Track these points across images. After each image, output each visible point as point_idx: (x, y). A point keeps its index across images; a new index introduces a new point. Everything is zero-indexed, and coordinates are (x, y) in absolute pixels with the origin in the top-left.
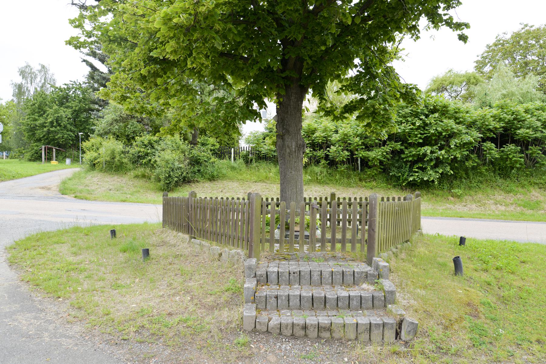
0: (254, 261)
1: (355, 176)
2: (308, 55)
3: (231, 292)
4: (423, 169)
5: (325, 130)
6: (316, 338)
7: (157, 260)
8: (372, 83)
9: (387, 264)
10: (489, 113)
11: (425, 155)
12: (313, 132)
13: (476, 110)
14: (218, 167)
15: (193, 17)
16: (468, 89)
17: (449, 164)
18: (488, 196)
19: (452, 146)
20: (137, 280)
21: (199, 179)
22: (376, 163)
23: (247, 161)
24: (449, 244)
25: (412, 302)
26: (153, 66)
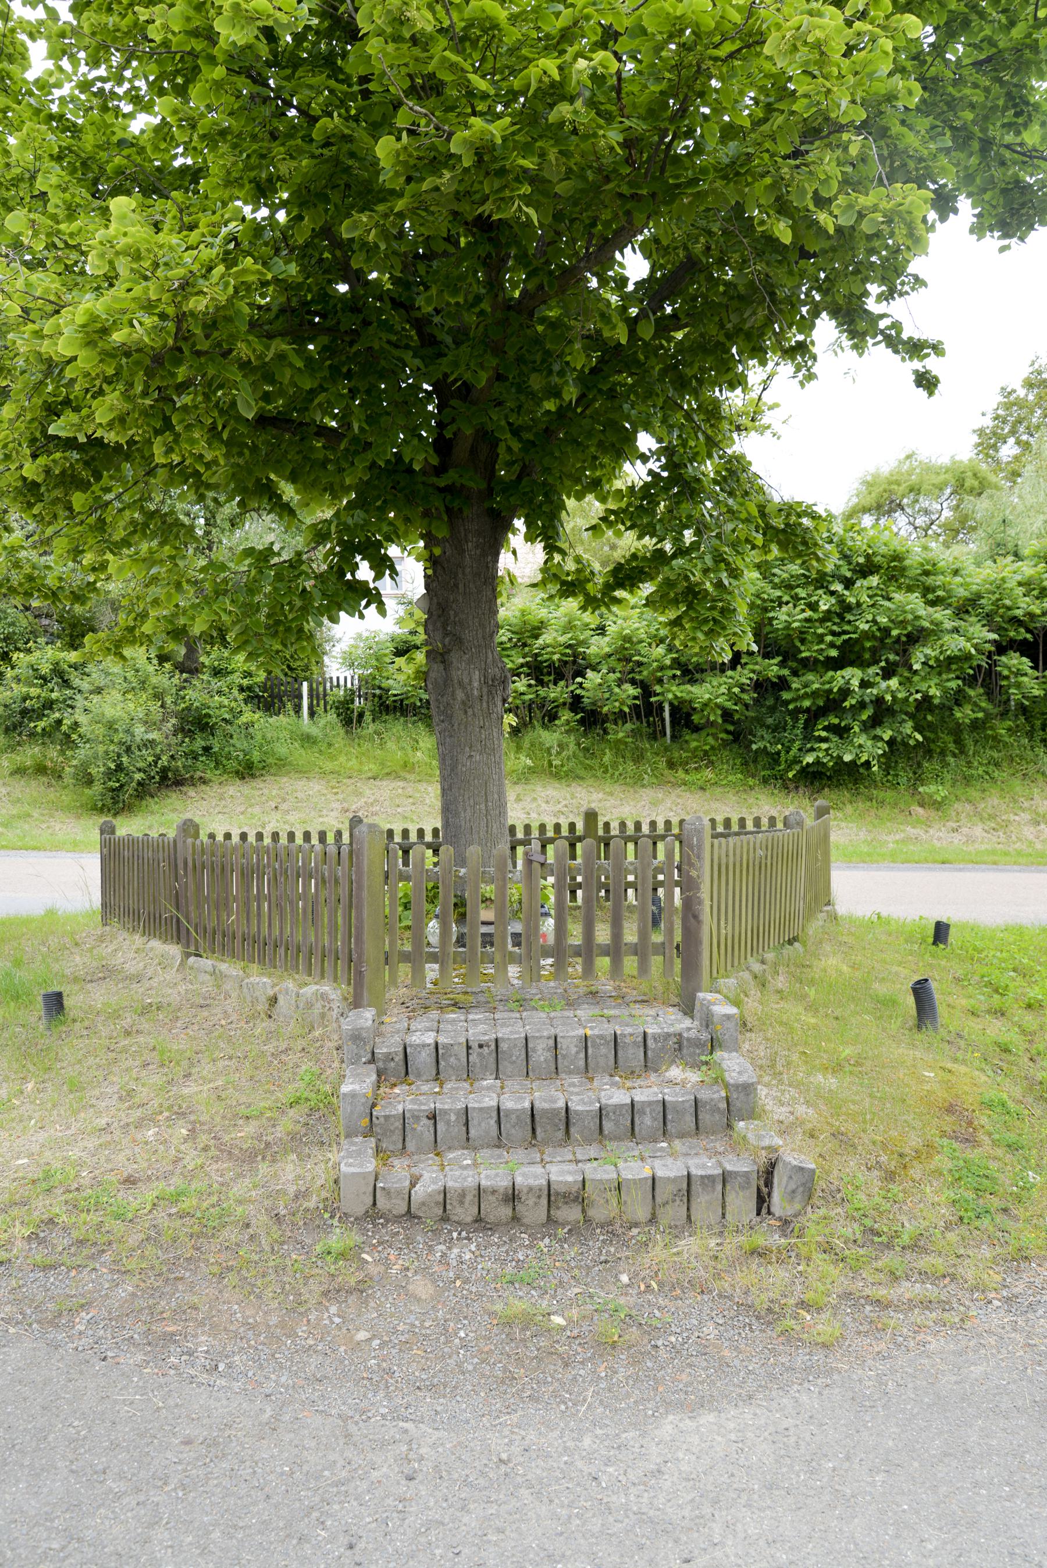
0: (367, 1015)
1: (657, 754)
2: (510, 424)
3: (304, 1108)
4: (842, 732)
5: (569, 627)
6: (543, 1225)
7: (86, 1023)
8: (686, 507)
9: (733, 1010)
10: (1013, 573)
11: (845, 692)
12: (537, 630)
13: (978, 564)
14: (264, 737)
15: (171, 326)
16: (958, 506)
17: (912, 716)
18: (1015, 801)
19: (916, 667)
20: (30, 1086)
21: (208, 775)
22: (712, 718)
23: (349, 718)
24: (906, 941)
25: (801, 1110)
26: (58, 455)
